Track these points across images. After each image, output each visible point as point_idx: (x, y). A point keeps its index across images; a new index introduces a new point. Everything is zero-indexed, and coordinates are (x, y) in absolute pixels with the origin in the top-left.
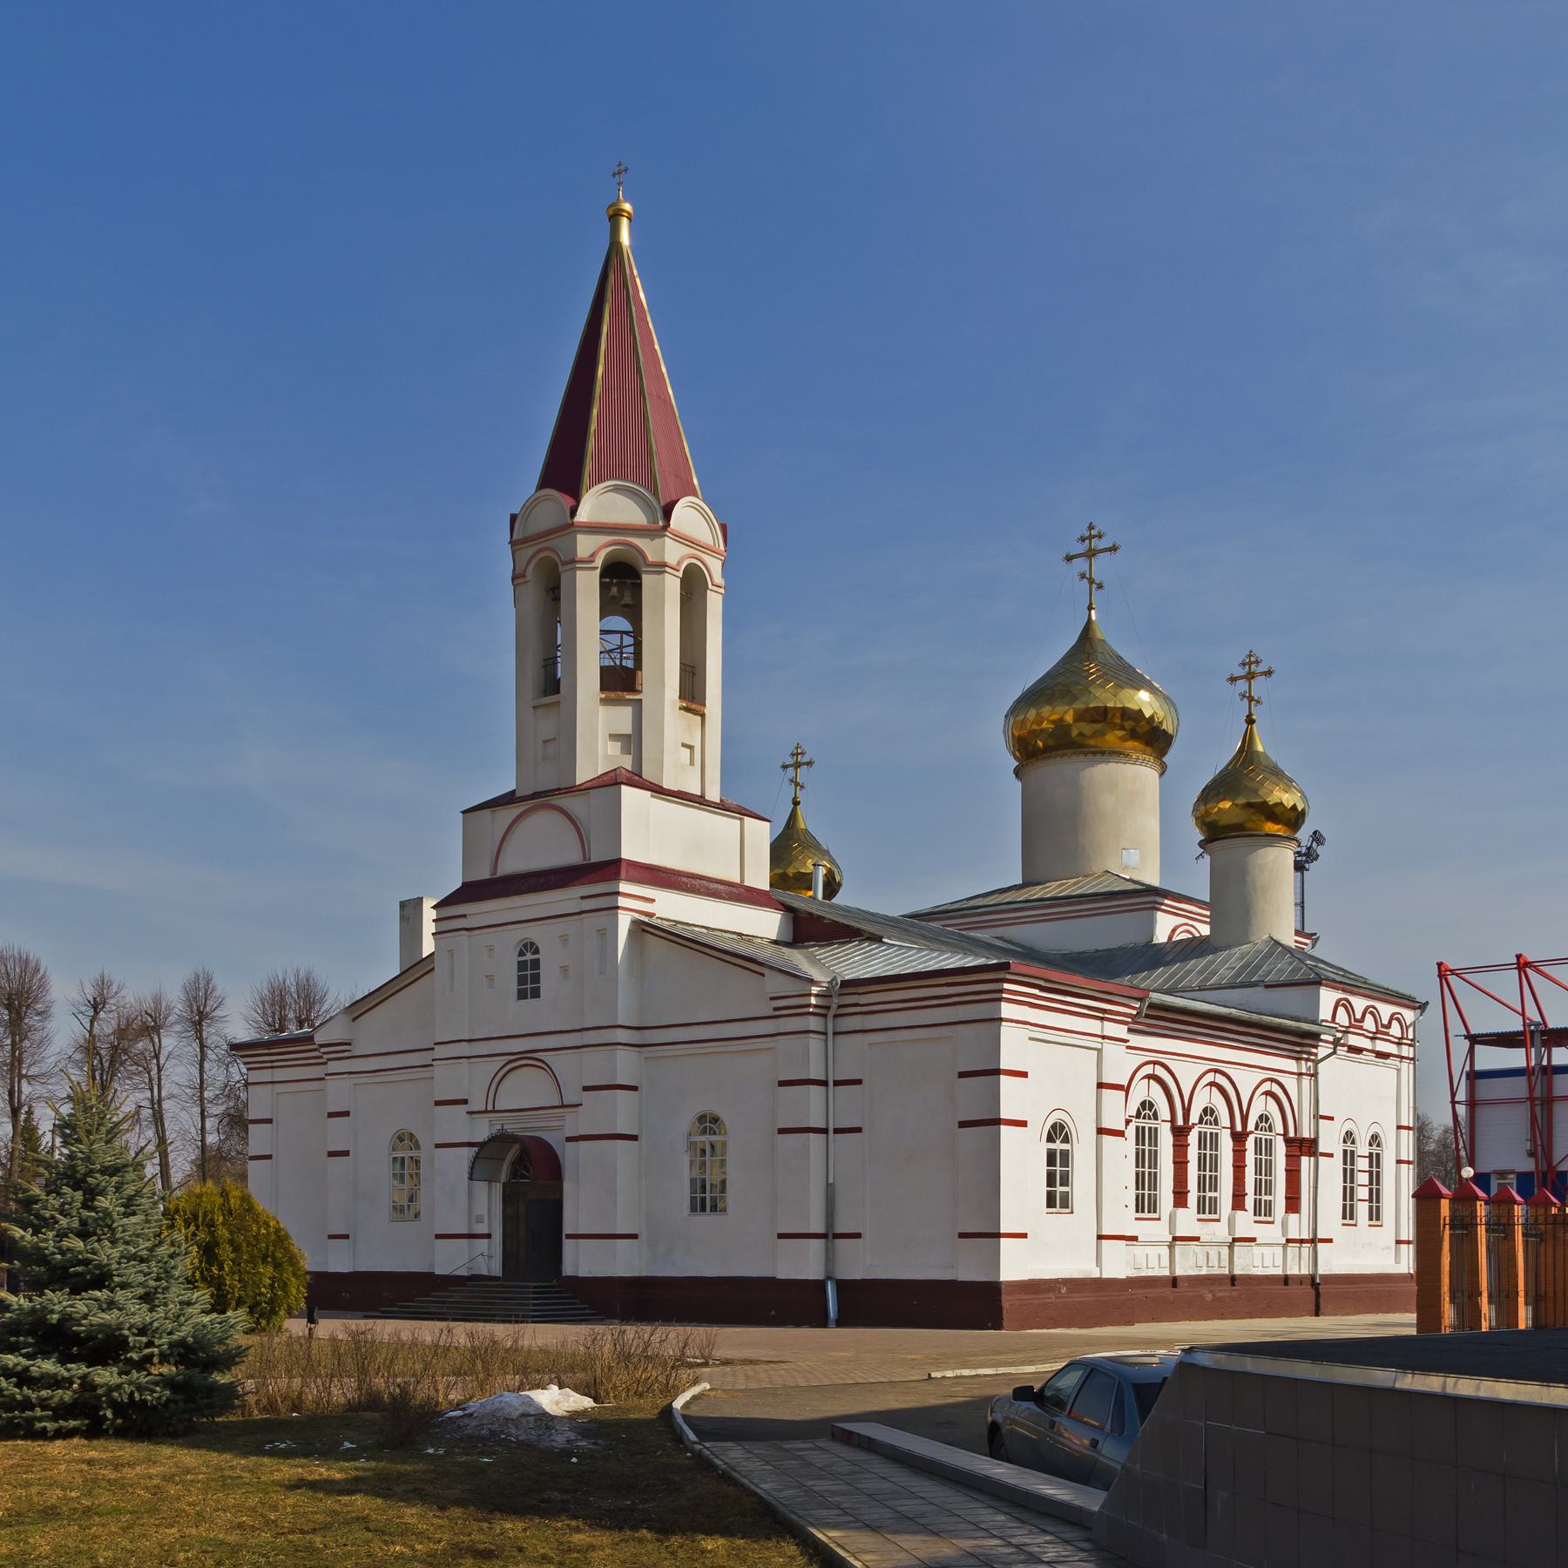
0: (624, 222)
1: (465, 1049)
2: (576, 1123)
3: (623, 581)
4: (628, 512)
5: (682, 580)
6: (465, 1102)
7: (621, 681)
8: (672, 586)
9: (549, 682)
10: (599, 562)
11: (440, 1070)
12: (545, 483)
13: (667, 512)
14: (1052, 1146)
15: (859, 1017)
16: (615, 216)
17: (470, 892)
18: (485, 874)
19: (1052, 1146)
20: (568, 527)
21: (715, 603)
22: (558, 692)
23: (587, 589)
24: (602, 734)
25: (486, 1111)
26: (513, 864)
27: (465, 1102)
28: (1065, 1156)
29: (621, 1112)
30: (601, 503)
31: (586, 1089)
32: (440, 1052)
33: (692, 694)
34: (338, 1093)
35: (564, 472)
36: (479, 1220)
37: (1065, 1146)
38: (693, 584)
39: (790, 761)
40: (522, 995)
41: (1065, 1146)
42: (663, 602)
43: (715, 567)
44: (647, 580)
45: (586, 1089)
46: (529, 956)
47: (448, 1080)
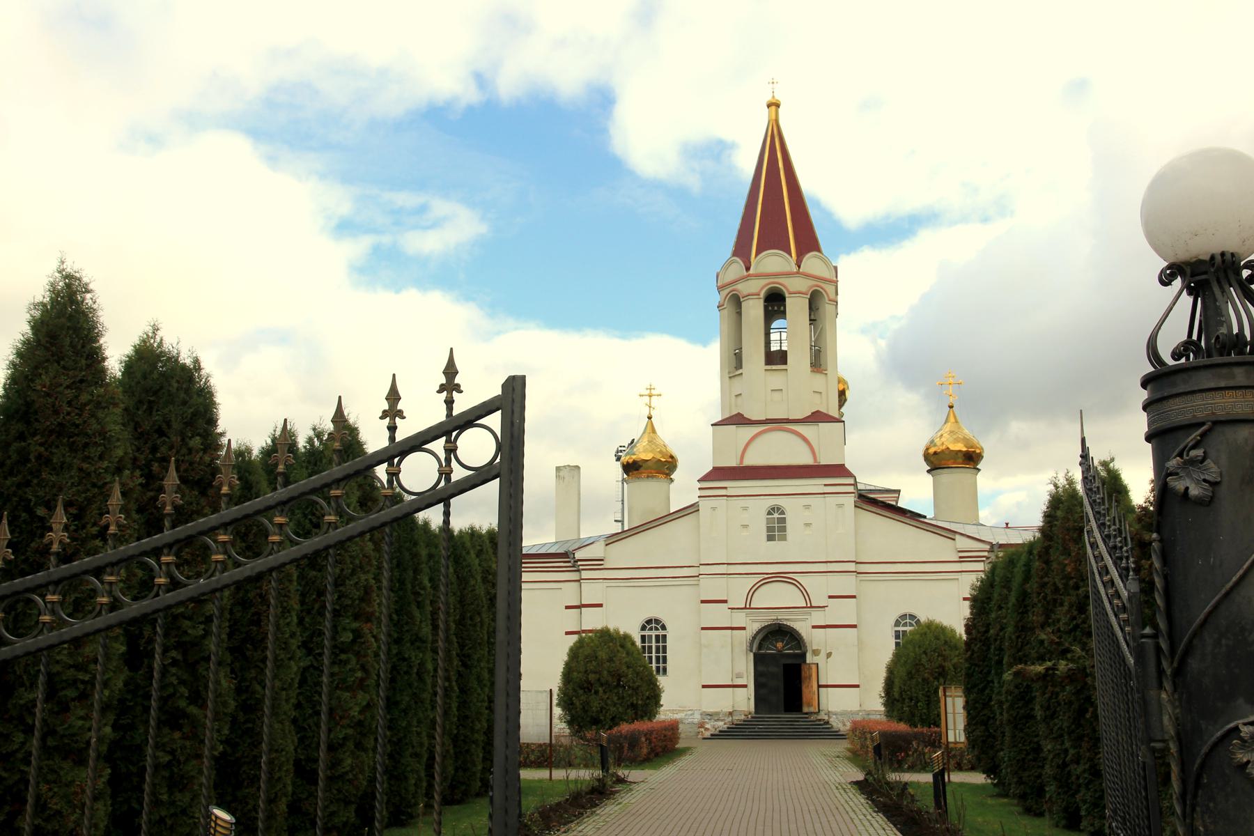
2: (818, 618)
6: (725, 602)
11: (704, 581)
12: (735, 254)
14: (643, 633)
15: (722, 581)
17: (719, 474)
18: (733, 463)
19: (643, 633)
22: (785, 363)
26: (752, 460)
27: (725, 602)
28: (664, 637)
29: (842, 612)
31: (830, 597)
32: (703, 570)
34: (591, 592)
36: (739, 676)
37: (663, 633)
40: (770, 538)
45: (830, 597)
47: (712, 588)
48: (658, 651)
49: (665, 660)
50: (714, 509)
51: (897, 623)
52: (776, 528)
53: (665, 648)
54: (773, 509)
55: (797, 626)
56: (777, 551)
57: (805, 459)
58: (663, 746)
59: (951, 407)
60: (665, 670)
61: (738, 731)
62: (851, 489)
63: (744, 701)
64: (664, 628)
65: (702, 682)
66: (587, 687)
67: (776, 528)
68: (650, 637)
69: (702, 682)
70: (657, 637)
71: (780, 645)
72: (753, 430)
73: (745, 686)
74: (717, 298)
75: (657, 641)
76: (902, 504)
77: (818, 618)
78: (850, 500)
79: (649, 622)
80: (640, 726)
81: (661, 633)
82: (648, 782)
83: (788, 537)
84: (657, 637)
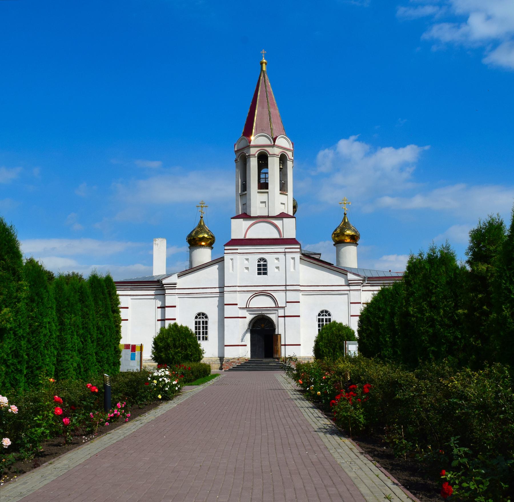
0: (264, 65)
1: (238, 289)
2: (281, 312)
3: (263, 160)
4: (264, 141)
5: (280, 158)
6: (237, 304)
7: (263, 186)
8: (277, 160)
9: (245, 187)
10: (256, 155)
13: (274, 140)
14: (319, 317)
16: (262, 64)
19: (319, 317)
20: (248, 146)
21: (290, 164)
22: (267, 188)
23: (254, 163)
24: (258, 202)
25: (246, 308)
26: (251, 235)
27: (237, 304)
28: (206, 322)
30: (256, 139)
33: (283, 188)
35: (248, 132)
37: (329, 317)
38: (283, 159)
39: (199, 205)
41: (329, 317)
42: (274, 164)
43: (290, 155)
44: (270, 159)
46: (262, 263)
48: (199, 327)
49: (206, 333)
50: (232, 259)
51: (319, 315)
52: (262, 269)
53: (206, 327)
54: (261, 260)
55: (271, 316)
56: (262, 280)
57: (275, 235)
58: (203, 373)
59: (201, 217)
60: (206, 339)
61: (243, 366)
62: (298, 250)
63: (245, 353)
64: (206, 317)
65: (228, 343)
66: (167, 347)
67: (262, 269)
68: (199, 322)
69: (228, 343)
70: (326, 319)
71: (263, 325)
72: (251, 222)
73: (246, 345)
74: (235, 157)
75: (203, 324)
76: (322, 258)
77: (281, 312)
78: (298, 256)
79: (199, 314)
80: (193, 365)
81: (205, 320)
82: (191, 391)
83: (268, 273)
84: (203, 322)
